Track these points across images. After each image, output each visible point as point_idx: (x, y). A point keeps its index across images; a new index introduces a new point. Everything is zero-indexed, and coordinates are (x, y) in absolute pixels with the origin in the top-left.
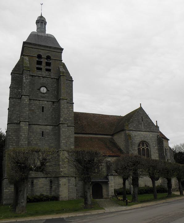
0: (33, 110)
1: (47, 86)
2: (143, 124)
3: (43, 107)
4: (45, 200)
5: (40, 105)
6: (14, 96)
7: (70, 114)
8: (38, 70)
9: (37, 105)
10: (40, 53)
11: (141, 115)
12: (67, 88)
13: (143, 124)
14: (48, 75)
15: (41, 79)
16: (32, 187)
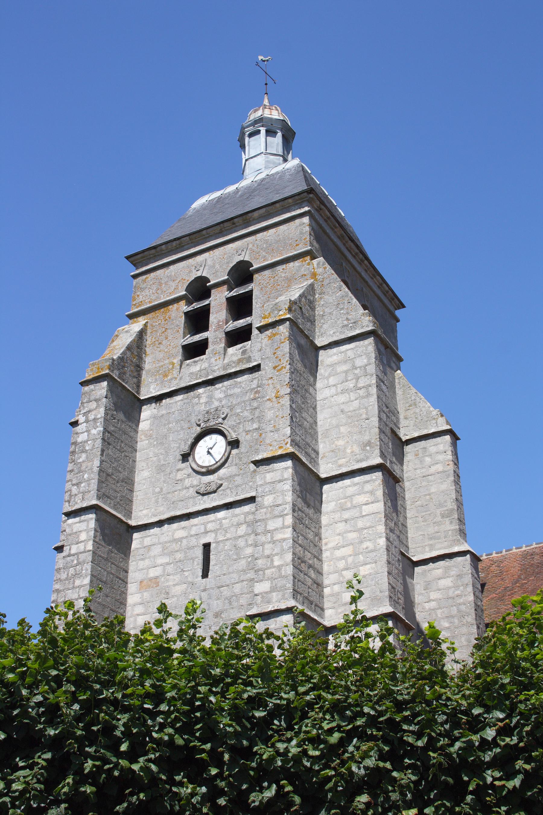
3: (207, 547)
5: (193, 541)
7: (361, 542)
12: (340, 388)
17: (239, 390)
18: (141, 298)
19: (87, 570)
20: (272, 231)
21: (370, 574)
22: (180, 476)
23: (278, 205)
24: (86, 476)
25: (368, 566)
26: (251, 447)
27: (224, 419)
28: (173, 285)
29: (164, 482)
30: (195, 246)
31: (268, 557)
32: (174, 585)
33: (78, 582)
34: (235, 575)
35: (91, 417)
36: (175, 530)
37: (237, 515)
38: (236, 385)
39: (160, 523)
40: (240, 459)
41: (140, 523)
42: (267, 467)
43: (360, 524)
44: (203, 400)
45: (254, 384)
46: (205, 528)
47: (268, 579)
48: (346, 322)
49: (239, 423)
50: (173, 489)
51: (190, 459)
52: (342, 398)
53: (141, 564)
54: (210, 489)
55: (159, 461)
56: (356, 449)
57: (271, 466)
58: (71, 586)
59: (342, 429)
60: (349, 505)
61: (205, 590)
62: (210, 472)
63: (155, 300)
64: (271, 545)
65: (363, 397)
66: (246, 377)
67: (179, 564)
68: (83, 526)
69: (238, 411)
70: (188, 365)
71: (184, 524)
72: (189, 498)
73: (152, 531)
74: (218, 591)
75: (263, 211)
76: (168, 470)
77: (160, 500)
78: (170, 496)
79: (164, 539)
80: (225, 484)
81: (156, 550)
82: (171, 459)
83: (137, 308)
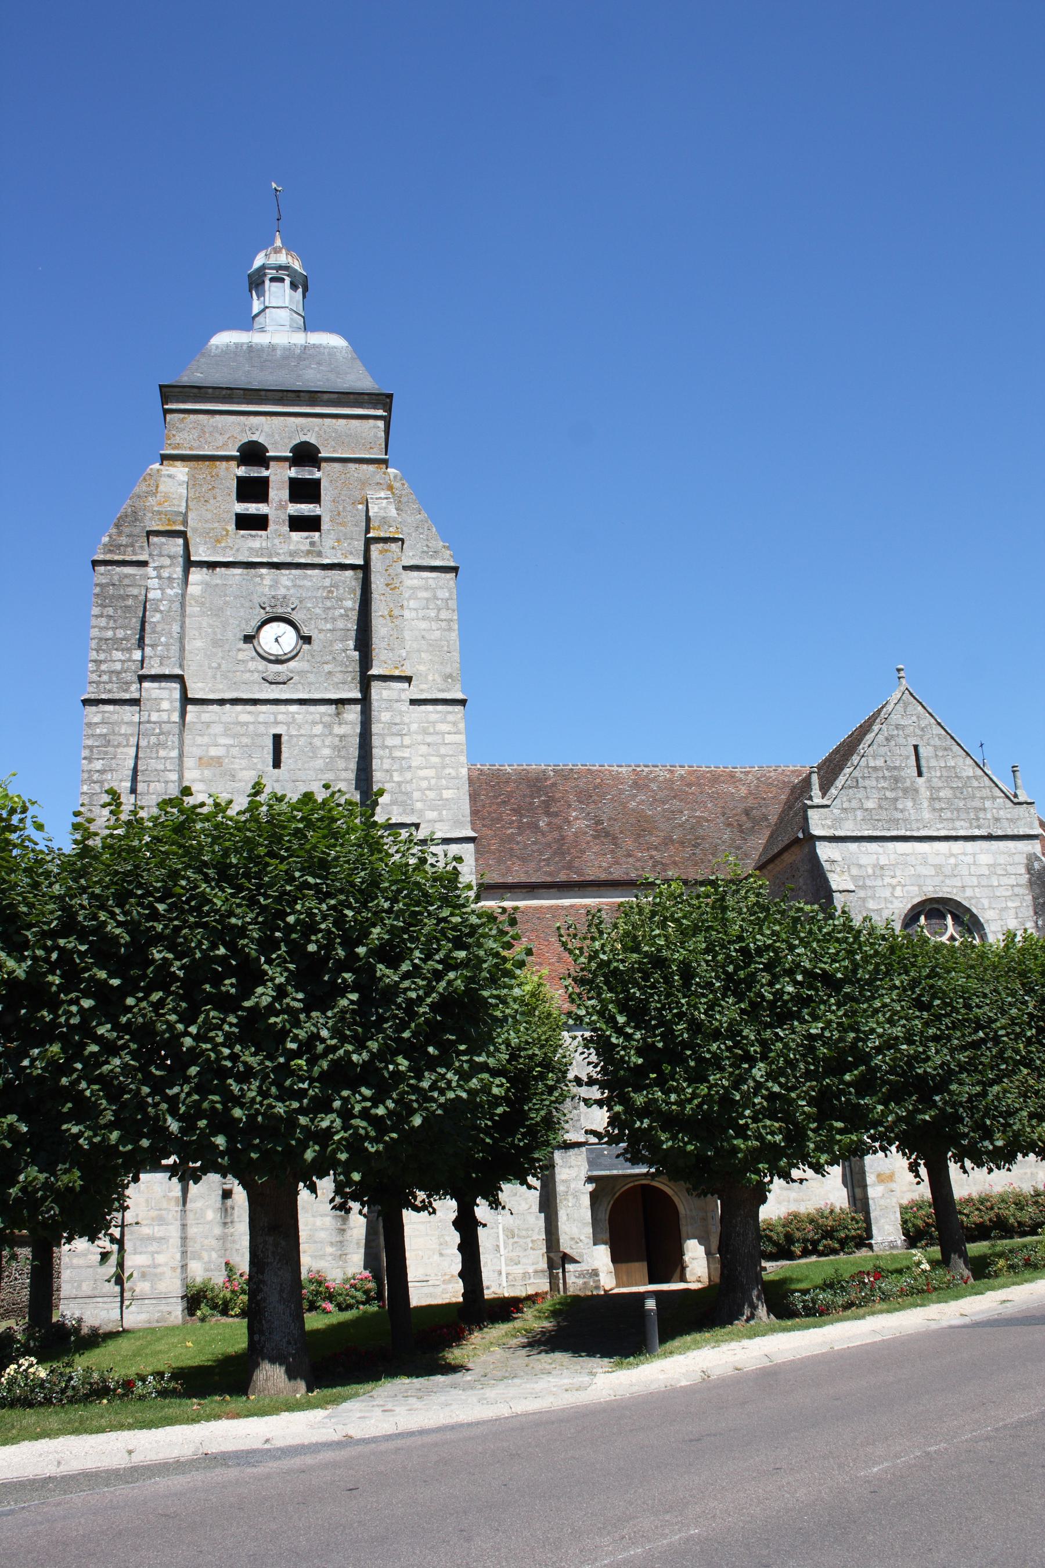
0: (218, 761)
1: (295, 617)
2: (925, 793)
3: (277, 739)
4: (123, 1257)
5: (262, 729)
6: (110, 691)
7: (444, 768)
8: (242, 532)
9: (242, 731)
10: (254, 438)
11: (906, 737)
12: (421, 613)
13: (925, 793)
14: (308, 547)
15: (261, 576)
16: (225, 1224)
17: (310, 584)
18: (177, 440)
19: (173, 742)
20: (342, 422)
21: (453, 799)
22: (241, 656)
23: (352, 396)
24: (163, 639)
25: (451, 791)
26: (325, 647)
27: (293, 609)
28: (221, 440)
29: (222, 658)
30: (248, 403)
31: (387, 771)
32: (241, 769)
33: (162, 753)
34: (311, 773)
35: (165, 574)
36: (240, 713)
37: (311, 713)
38: (306, 577)
39: (222, 702)
40: (313, 656)
41: (197, 697)
42: (383, 684)
43: (443, 750)
44: (267, 582)
45: (327, 582)
46: (275, 718)
48: (425, 549)
49: (311, 619)
50: (234, 669)
51: (255, 642)
52: (424, 625)
53: (199, 740)
55: (215, 633)
56: (439, 680)
57: (388, 683)
58: (154, 755)
59: (423, 655)
60: (431, 730)
61: (277, 781)
62: (278, 661)
63: (197, 449)
64: (389, 761)
65: (445, 630)
66: (317, 572)
67: (245, 749)
68: (165, 694)
69: (309, 605)
70: (243, 536)
71: (249, 708)
72: (254, 682)
73: (210, 707)
74: (292, 784)
75: (336, 396)
76: (227, 647)
77: (218, 676)
78: (230, 675)
79: (225, 718)
81: (217, 729)
82: (230, 635)
83: (173, 449)
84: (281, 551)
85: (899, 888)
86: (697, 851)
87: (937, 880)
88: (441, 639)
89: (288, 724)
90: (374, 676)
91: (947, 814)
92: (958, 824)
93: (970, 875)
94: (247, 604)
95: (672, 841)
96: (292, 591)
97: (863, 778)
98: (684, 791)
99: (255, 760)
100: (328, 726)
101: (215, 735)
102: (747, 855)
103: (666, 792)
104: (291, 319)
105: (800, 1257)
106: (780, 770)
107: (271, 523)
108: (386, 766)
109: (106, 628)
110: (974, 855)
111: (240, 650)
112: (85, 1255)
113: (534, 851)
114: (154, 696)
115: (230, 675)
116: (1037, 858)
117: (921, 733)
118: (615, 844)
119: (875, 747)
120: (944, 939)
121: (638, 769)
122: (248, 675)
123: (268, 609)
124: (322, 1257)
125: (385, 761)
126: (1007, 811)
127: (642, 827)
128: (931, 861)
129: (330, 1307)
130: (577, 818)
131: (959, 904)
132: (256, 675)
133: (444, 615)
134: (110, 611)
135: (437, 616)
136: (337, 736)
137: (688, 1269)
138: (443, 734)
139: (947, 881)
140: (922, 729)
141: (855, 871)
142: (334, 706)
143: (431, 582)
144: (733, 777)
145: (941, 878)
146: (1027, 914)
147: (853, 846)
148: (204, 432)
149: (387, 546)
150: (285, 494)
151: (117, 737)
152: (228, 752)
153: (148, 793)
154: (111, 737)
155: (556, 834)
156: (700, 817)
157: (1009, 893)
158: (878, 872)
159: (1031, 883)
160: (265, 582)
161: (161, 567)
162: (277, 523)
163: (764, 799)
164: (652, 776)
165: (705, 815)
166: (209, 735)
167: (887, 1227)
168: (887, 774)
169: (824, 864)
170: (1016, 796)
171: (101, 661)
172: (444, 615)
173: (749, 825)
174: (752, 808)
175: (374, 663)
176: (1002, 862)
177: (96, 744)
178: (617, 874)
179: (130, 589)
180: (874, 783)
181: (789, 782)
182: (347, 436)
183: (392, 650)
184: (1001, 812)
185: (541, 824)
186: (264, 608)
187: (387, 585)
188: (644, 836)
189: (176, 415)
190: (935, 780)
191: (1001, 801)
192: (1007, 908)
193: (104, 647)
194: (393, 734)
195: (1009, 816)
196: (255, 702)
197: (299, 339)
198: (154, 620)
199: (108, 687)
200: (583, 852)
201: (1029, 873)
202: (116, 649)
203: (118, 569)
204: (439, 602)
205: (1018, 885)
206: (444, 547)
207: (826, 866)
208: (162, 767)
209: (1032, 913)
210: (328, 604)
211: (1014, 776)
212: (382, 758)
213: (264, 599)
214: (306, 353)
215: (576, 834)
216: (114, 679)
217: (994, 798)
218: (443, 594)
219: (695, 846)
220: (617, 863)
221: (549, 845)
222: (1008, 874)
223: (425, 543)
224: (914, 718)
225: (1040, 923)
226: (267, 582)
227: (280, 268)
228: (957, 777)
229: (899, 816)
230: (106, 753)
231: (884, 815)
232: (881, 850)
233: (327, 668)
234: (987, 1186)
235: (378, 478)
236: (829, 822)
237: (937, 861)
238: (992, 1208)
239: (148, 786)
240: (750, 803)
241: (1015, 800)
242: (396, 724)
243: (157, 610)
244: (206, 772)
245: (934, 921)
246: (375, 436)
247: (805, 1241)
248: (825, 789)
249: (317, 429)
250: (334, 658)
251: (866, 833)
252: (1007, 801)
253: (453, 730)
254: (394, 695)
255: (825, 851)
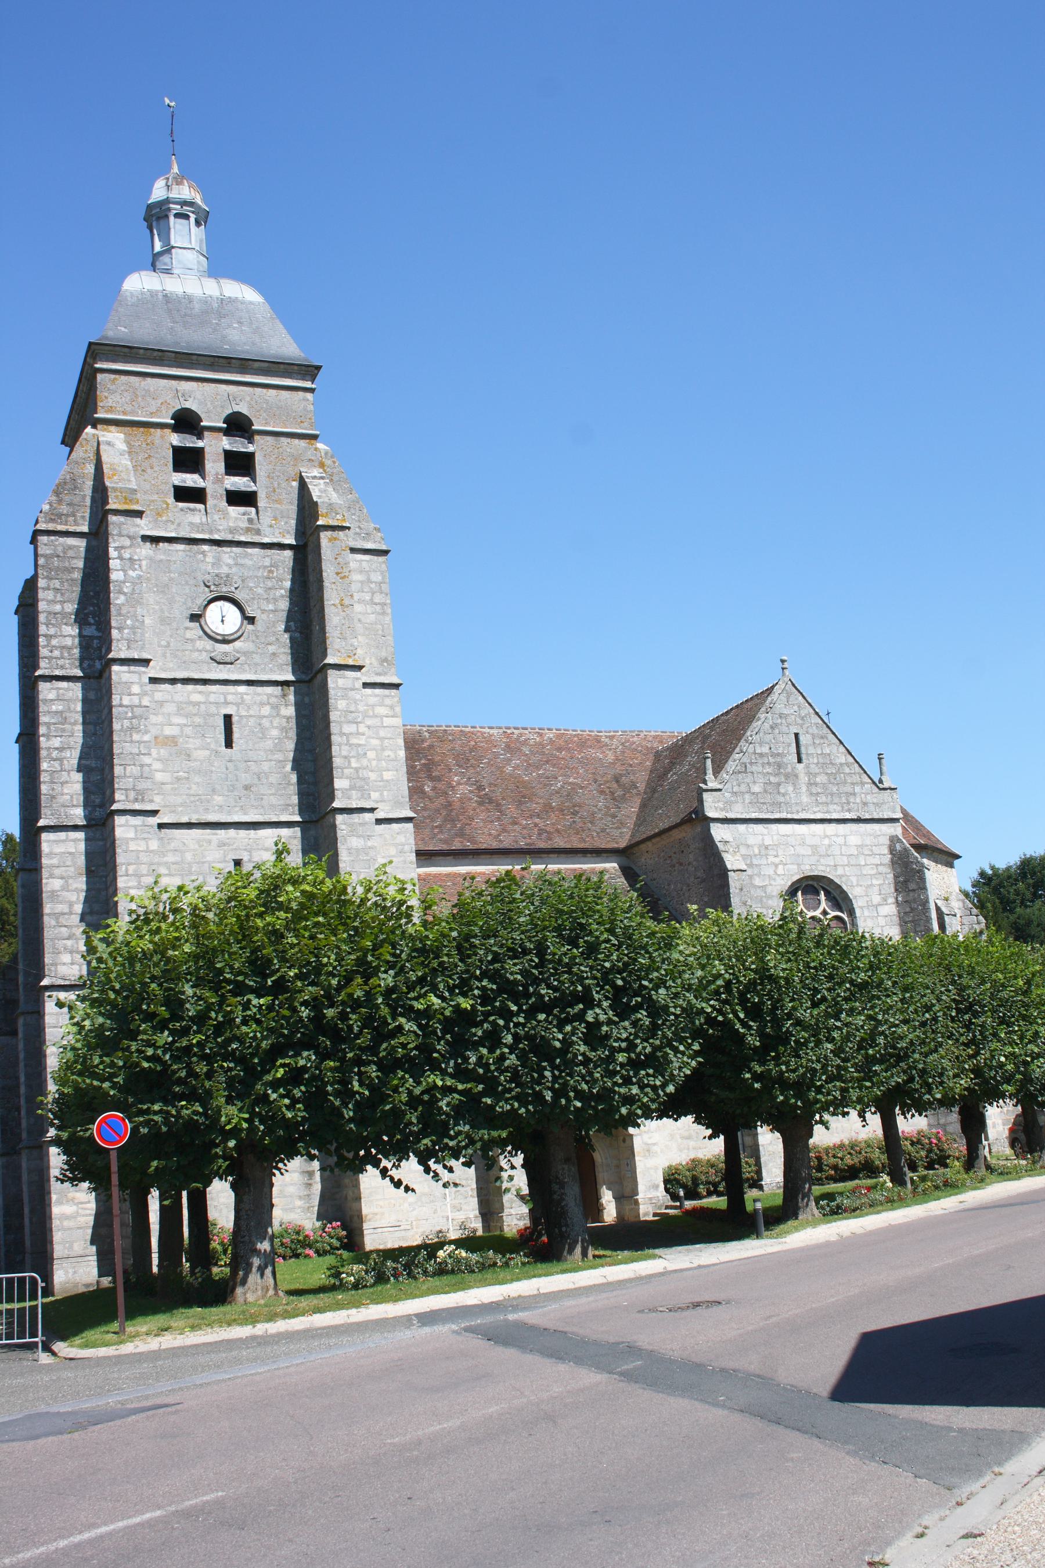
0: (172, 741)
1: (239, 596)
2: (803, 779)
3: (228, 719)
5: (213, 709)
7: (383, 750)
8: (181, 505)
13: (803, 779)
14: (245, 525)
15: (203, 553)
17: (251, 563)
22: (189, 634)
23: (282, 366)
24: (129, 622)
25: (390, 773)
28: (154, 406)
29: (171, 636)
30: (177, 367)
31: (346, 757)
32: (196, 749)
33: (136, 737)
36: (191, 692)
37: (259, 694)
38: (247, 555)
39: (173, 681)
40: (257, 637)
43: (382, 733)
44: (209, 559)
45: (267, 562)
46: (225, 699)
47: (347, 778)
49: (253, 599)
54: (228, 660)
55: (162, 611)
56: (375, 663)
58: (129, 739)
61: (230, 761)
62: (225, 641)
65: (379, 614)
67: (198, 728)
69: (251, 585)
70: (182, 510)
71: (200, 688)
72: (203, 662)
75: (266, 365)
76: (174, 625)
77: (168, 655)
78: (179, 654)
79: (178, 698)
80: (242, 658)
81: (170, 708)
84: (221, 528)
85: (781, 867)
86: (577, 819)
87: (813, 860)
88: (376, 623)
89: (237, 705)
90: (330, 665)
91: (822, 799)
92: (832, 807)
93: (841, 855)
94: (192, 582)
95: (552, 808)
96: (234, 570)
97: (751, 763)
98: (555, 756)
99: (209, 740)
100: (275, 707)
101: (169, 714)
102: (622, 824)
103: (538, 757)
104: (198, 262)
105: (705, 1197)
106: (642, 735)
107: (209, 497)
108: (344, 753)
109: (54, 602)
110: (845, 836)
111: (187, 628)
112: (75, 1217)
113: (425, 818)
114: (124, 680)
115: (179, 654)
116: (899, 840)
117: (801, 722)
118: (500, 811)
119: (761, 734)
120: (817, 913)
121: (509, 731)
122: (196, 654)
123: (212, 587)
124: (292, 1210)
125: (343, 747)
126: (874, 796)
127: (522, 794)
128: (808, 842)
129: (311, 1252)
130: (459, 784)
131: (831, 881)
132: (204, 654)
133: (378, 598)
134: (56, 584)
135: (372, 599)
136: (284, 717)
137: (605, 1211)
138: (382, 717)
139: (822, 860)
140: (802, 719)
141: (743, 850)
142: (280, 688)
143: (364, 564)
144: (599, 741)
145: (816, 857)
146: (889, 891)
147: (742, 828)
148: (137, 396)
149: (335, 534)
150: (221, 467)
151: (73, 715)
152: (182, 731)
153: (125, 776)
154: (68, 714)
155: (442, 800)
156: (574, 784)
157: (874, 872)
158: (763, 852)
159: (893, 862)
160: (207, 560)
161: (122, 547)
162: (215, 497)
163: (631, 765)
164: (523, 739)
165: (579, 781)
166: (163, 714)
167: (774, 1170)
168: (771, 760)
169: (718, 844)
170: (881, 781)
171: (51, 636)
172: (378, 598)
173: (619, 793)
174: (621, 775)
175: (329, 651)
176: (868, 843)
177: (53, 721)
178: (507, 842)
179: (75, 561)
180: (760, 769)
181: (652, 748)
182: (279, 408)
183: (345, 639)
184: (869, 797)
185: (427, 789)
186: (208, 587)
187: (337, 574)
188: (526, 802)
189: (107, 375)
190: (813, 766)
191: (869, 786)
192: (872, 885)
193: (53, 621)
194: (350, 722)
195: (875, 801)
196: (205, 682)
197: (211, 288)
198: (118, 602)
199: (61, 662)
200: (471, 819)
201: (891, 853)
202: (66, 624)
203: (61, 540)
204: (373, 586)
205: (881, 864)
206: (375, 529)
207: (720, 846)
208: (136, 751)
209: (893, 890)
210: (269, 584)
211: (880, 763)
212: (340, 745)
213: (208, 577)
214: (225, 307)
215: (461, 800)
216: (66, 655)
217: (863, 784)
218: (377, 577)
219: (575, 813)
220: (504, 830)
221: (437, 811)
222: (873, 854)
223: (357, 524)
224: (796, 708)
225: (900, 899)
226: (209, 559)
227: (184, 203)
228: (831, 763)
229: (781, 799)
230: (63, 730)
231: (768, 798)
232: (765, 831)
233: (271, 649)
234: (853, 1134)
235: (310, 454)
236: (721, 805)
237: (815, 841)
238: (860, 1153)
239: (125, 769)
240: (619, 769)
241: (881, 786)
242: (351, 712)
243: (120, 592)
244: (162, 751)
245: (809, 897)
246: (305, 409)
247: (708, 1183)
248: (716, 772)
249: (248, 399)
250: (277, 639)
251: (753, 816)
252: (874, 787)
253: (391, 713)
254: (348, 683)
255: (718, 832)
